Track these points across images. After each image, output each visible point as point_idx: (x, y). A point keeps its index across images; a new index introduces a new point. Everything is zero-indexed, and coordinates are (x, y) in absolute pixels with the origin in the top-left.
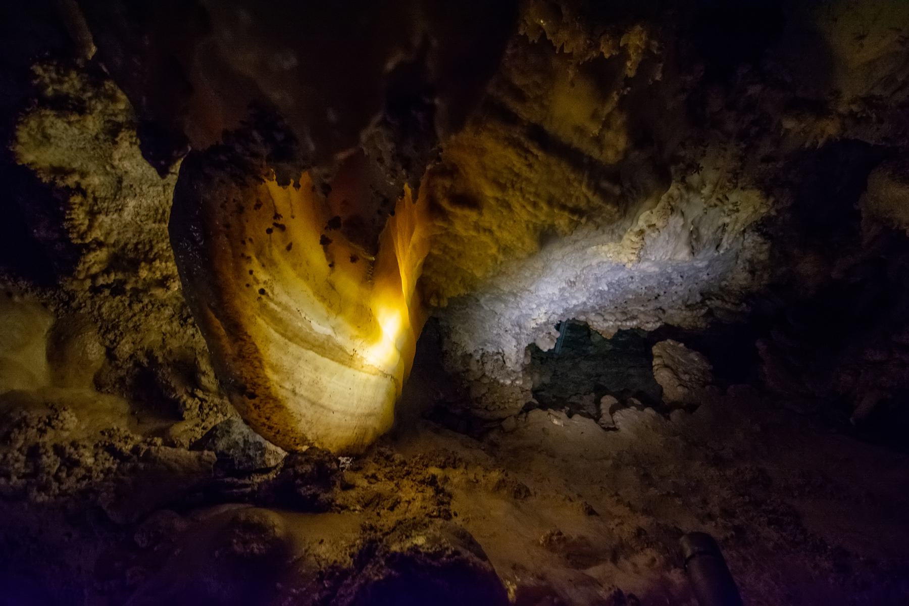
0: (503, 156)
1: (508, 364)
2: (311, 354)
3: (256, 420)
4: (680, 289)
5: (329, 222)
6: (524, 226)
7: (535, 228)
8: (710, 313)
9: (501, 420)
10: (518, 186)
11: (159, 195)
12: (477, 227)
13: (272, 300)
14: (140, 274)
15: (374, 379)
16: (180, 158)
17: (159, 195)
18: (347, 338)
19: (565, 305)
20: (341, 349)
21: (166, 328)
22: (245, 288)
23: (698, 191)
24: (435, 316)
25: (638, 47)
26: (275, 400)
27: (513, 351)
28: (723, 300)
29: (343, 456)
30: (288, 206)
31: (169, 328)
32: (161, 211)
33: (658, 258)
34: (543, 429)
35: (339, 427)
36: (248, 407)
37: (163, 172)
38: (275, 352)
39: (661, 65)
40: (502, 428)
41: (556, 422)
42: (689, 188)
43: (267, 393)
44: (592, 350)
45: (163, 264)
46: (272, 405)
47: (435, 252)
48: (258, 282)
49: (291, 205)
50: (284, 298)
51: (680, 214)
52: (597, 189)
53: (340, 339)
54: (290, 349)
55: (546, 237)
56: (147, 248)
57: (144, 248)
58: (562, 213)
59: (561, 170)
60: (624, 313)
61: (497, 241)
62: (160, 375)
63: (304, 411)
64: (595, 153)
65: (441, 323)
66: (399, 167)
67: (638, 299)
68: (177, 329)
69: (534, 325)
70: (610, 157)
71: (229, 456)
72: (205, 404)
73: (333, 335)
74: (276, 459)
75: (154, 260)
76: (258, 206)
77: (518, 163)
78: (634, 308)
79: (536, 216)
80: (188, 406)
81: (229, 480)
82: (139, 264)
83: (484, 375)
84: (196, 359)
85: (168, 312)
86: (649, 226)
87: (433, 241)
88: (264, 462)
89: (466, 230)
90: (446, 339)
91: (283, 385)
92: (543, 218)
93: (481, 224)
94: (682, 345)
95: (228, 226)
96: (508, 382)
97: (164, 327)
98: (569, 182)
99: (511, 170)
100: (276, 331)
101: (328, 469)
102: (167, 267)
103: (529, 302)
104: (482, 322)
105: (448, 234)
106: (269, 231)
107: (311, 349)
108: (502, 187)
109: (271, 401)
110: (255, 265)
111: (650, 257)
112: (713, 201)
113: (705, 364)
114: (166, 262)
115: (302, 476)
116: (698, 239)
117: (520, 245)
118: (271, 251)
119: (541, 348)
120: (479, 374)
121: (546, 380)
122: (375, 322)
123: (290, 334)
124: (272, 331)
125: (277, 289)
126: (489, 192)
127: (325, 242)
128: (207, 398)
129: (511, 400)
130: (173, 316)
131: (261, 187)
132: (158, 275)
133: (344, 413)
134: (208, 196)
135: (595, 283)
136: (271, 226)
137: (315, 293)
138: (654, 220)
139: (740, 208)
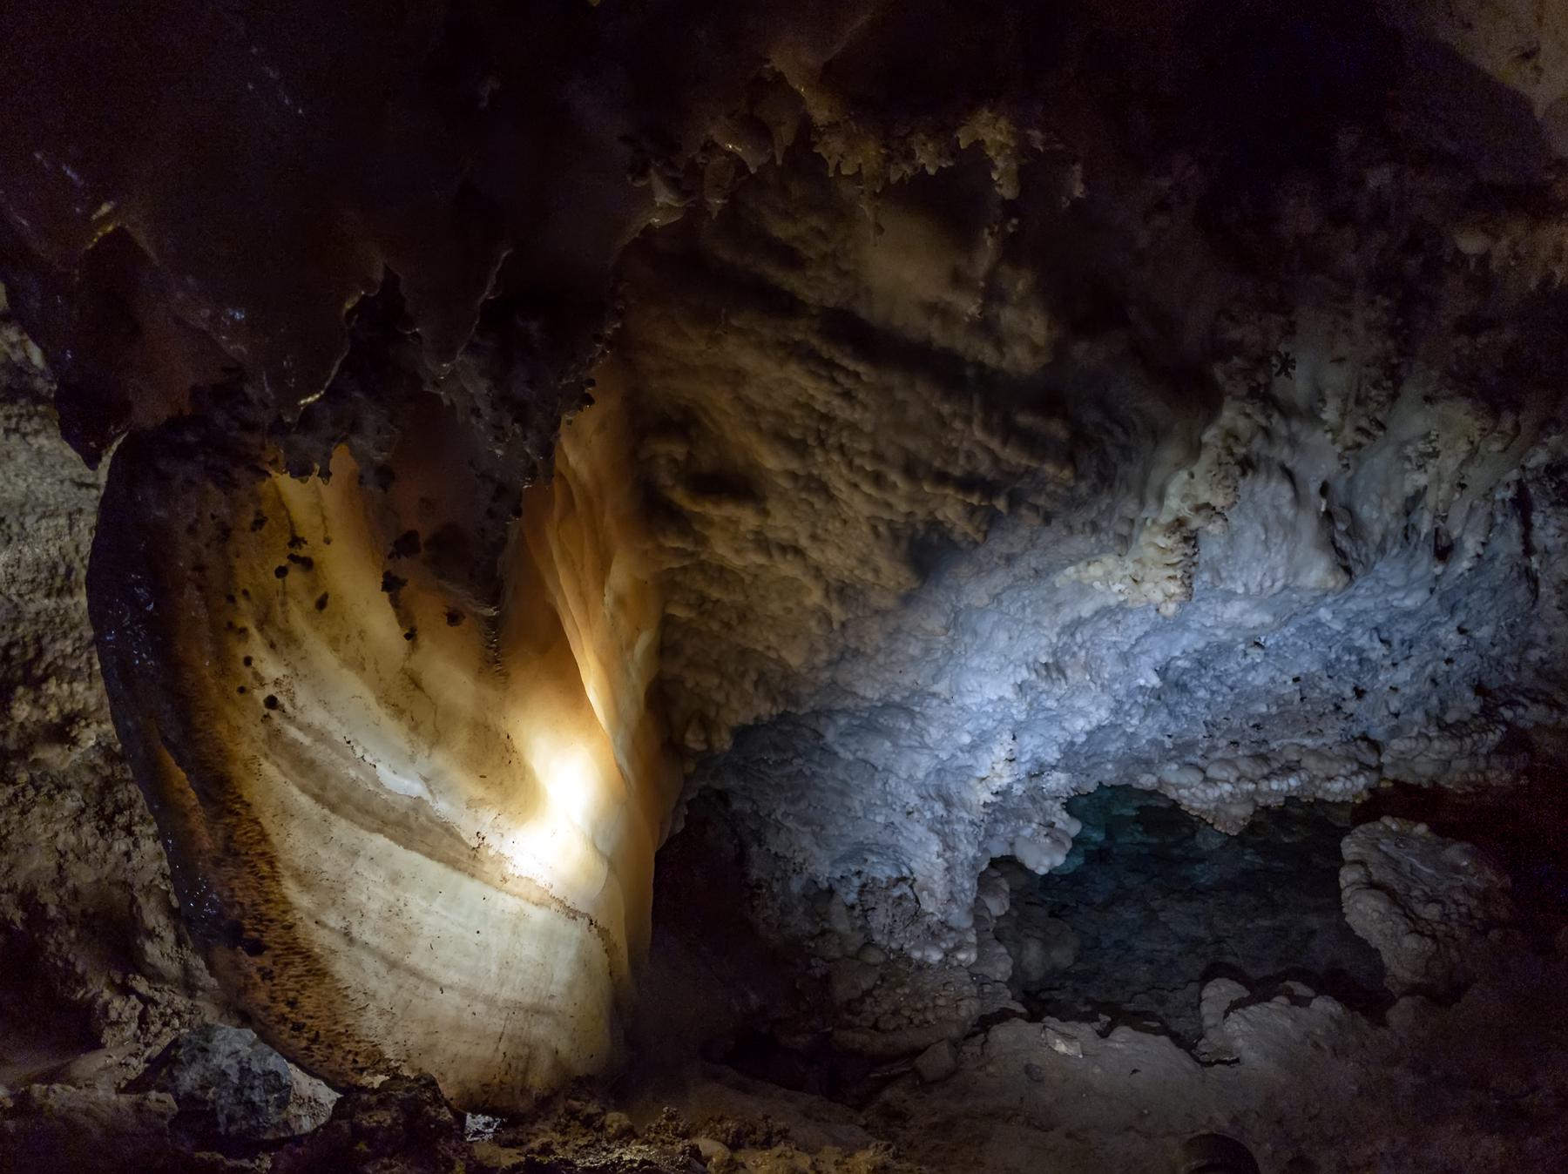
0: (788, 384)
1: (929, 906)
2: (380, 842)
3: (266, 1008)
4: (1403, 674)
5: (396, 544)
6: (865, 529)
7: (896, 536)
8: (1516, 741)
9: (917, 1052)
10: (832, 441)
11: (59, 536)
12: (762, 543)
13: (291, 720)
14: (14, 712)
15: (538, 916)
16: (119, 435)
17: (59, 536)
18: (457, 802)
19: (1062, 737)
20: (449, 830)
21: (66, 839)
22: (236, 695)
23: (1311, 416)
24: (718, 786)
25: (1003, 146)
26: (307, 956)
27: (933, 865)
28: (1552, 704)
29: (475, 1112)
30: (317, 520)
31: (72, 839)
32: (62, 570)
33: (1254, 589)
34: (1028, 1069)
35: (458, 1028)
36: (248, 976)
37: (92, 460)
38: (301, 836)
39: (1078, 167)
40: (916, 1073)
41: (1061, 1047)
42: (1287, 411)
43: (288, 939)
44: (1203, 875)
45: (65, 686)
46: (301, 969)
47: (680, 612)
48: (262, 683)
49: (324, 518)
50: (317, 716)
51: (1277, 474)
52: (1010, 432)
53: (443, 807)
54: (336, 832)
55: (927, 555)
56: (31, 654)
57: (25, 653)
58: (940, 491)
59: (920, 398)
60: (1263, 758)
61: (817, 572)
62: (52, 948)
63: (373, 984)
64: (988, 355)
65: (736, 806)
66: (507, 422)
67: (1286, 716)
68: (91, 842)
69: (986, 797)
70: (1021, 359)
71: (205, 1102)
72: (152, 1011)
73: (427, 796)
74: (314, 1116)
75: (45, 679)
76: (259, 523)
77: (821, 394)
78: (1284, 742)
79: (889, 505)
80: (113, 1015)
81: (205, 1155)
82: (12, 690)
83: (869, 943)
84: (134, 900)
85: (71, 803)
86: (1198, 509)
87: (667, 586)
88: (286, 1123)
89: (738, 551)
90: (755, 848)
91: (323, 918)
92: (903, 507)
93: (770, 535)
94: (1421, 829)
95: (200, 568)
96: (935, 956)
97: (61, 838)
98: (943, 423)
99: (808, 408)
100: (304, 790)
101: (431, 1120)
102: (72, 694)
103: (950, 729)
104: (842, 793)
105: (702, 566)
106: (281, 572)
107: (380, 831)
108: (798, 448)
109: (297, 959)
110: (256, 646)
111: (1231, 586)
112: (1349, 435)
113: (1489, 873)
114: (70, 683)
115: (369, 1135)
116: (1356, 530)
117: (869, 576)
118: (286, 613)
119: (1030, 865)
120: (859, 938)
121: (1063, 957)
122: (522, 765)
123: (332, 796)
124: (295, 791)
125: (302, 697)
126: (772, 461)
127: (391, 584)
128: (157, 996)
129: (941, 1002)
130: (83, 811)
131: (265, 486)
132: (53, 711)
133: (469, 993)
134: (162, 513)
135: (1120, 669)
136: (284, 562)
137: (379, 699)
138: (1205, 496)
139: (1438, 446)
